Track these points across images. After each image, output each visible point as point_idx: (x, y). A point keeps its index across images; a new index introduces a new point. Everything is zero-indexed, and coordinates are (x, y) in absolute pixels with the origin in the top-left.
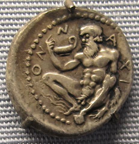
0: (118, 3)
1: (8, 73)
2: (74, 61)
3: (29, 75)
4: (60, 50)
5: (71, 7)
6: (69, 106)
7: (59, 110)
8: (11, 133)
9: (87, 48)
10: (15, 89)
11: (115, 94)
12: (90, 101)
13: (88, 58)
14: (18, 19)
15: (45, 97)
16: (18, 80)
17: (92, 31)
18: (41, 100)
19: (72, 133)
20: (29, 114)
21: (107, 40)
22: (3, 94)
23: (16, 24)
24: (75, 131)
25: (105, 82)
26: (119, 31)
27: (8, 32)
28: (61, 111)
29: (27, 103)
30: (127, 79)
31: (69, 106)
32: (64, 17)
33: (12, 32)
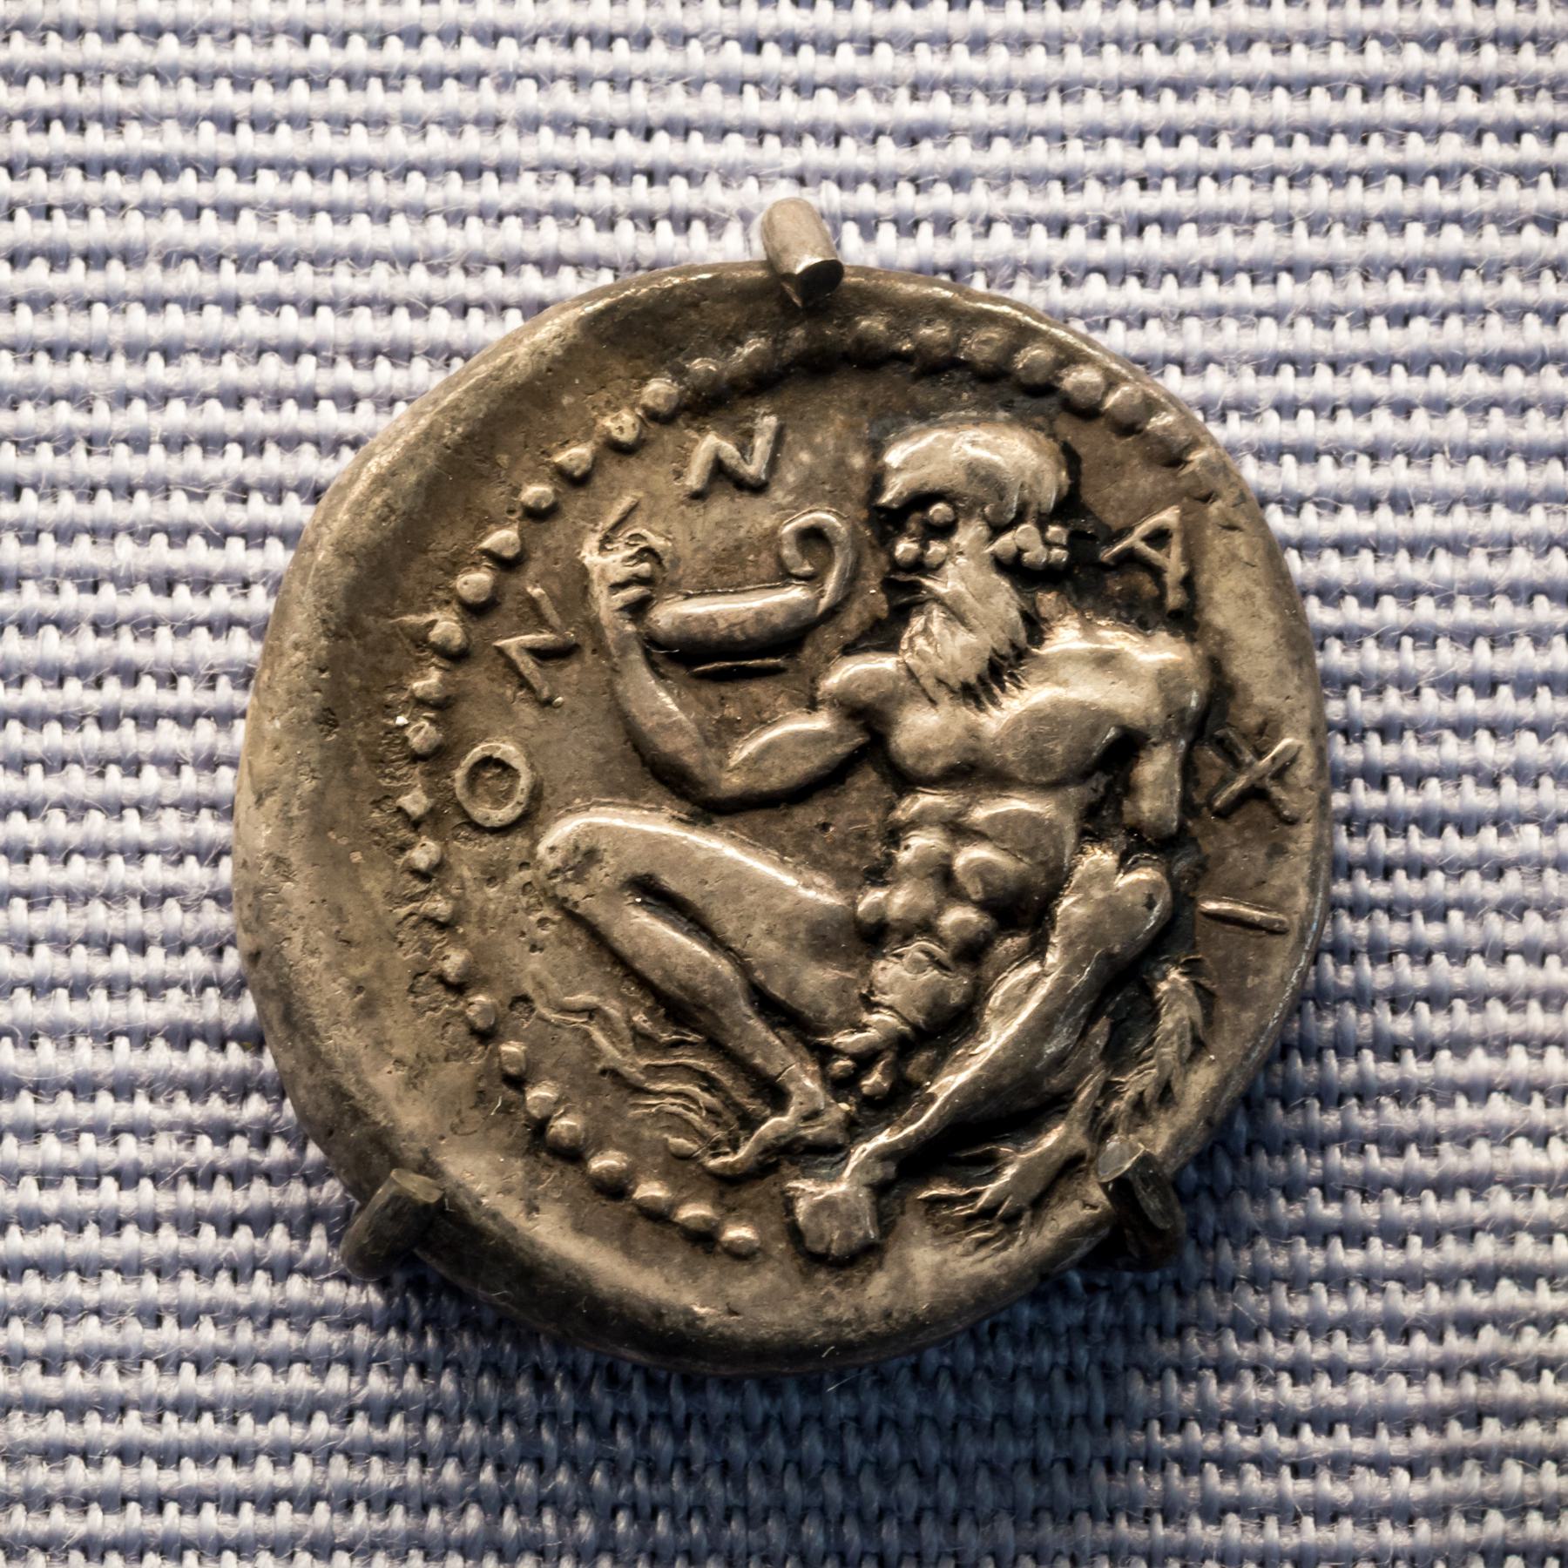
1: (252, 799)
2: (821, 722)
3: (423, 828)
4: (695, 629)
5: (799, 270)
6: (752, 1105)
7: (669, 1129)
8: (261, 1319)
9: (929, 620)
10: (297, 937)
11: (1155, 1017)
12: (933, 1071)
13: (933, 702)
14: (363, 354)
15: (554, 1017)
16: (332, 863)
17: (986, 478)
18: (517, 1036)
19: (763, 1333)
20: (412, 1152)
21: (1107, 554)
22: (206, 983)
23: (348, 400)
24: (793, 1311)
25: (1067, 916)
26: (1219, 484)
27: (274, 463)
28: (680, 1142)
29: (399, 1062)
30: (1269, 894)
31: (752, 1105)
32: (752, 346)
33: (308, 463)
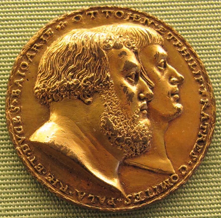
0: (203, 2)
